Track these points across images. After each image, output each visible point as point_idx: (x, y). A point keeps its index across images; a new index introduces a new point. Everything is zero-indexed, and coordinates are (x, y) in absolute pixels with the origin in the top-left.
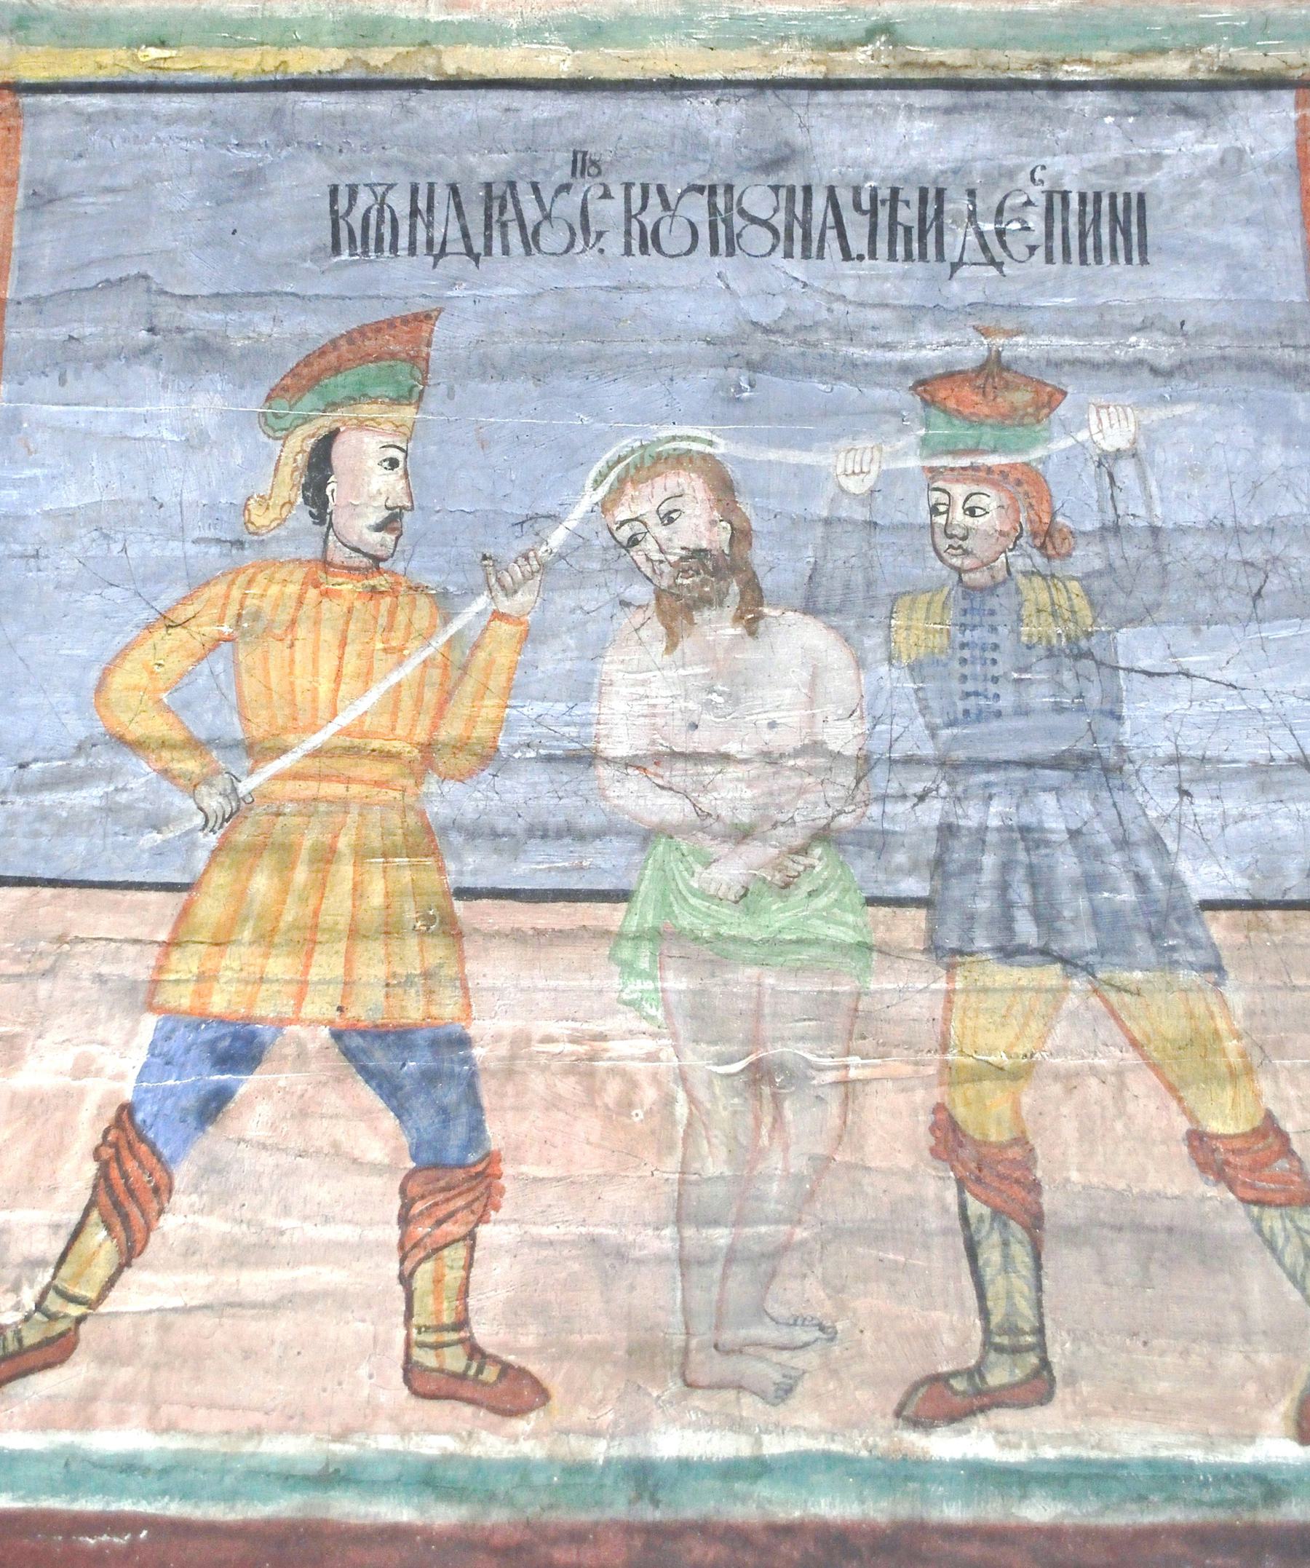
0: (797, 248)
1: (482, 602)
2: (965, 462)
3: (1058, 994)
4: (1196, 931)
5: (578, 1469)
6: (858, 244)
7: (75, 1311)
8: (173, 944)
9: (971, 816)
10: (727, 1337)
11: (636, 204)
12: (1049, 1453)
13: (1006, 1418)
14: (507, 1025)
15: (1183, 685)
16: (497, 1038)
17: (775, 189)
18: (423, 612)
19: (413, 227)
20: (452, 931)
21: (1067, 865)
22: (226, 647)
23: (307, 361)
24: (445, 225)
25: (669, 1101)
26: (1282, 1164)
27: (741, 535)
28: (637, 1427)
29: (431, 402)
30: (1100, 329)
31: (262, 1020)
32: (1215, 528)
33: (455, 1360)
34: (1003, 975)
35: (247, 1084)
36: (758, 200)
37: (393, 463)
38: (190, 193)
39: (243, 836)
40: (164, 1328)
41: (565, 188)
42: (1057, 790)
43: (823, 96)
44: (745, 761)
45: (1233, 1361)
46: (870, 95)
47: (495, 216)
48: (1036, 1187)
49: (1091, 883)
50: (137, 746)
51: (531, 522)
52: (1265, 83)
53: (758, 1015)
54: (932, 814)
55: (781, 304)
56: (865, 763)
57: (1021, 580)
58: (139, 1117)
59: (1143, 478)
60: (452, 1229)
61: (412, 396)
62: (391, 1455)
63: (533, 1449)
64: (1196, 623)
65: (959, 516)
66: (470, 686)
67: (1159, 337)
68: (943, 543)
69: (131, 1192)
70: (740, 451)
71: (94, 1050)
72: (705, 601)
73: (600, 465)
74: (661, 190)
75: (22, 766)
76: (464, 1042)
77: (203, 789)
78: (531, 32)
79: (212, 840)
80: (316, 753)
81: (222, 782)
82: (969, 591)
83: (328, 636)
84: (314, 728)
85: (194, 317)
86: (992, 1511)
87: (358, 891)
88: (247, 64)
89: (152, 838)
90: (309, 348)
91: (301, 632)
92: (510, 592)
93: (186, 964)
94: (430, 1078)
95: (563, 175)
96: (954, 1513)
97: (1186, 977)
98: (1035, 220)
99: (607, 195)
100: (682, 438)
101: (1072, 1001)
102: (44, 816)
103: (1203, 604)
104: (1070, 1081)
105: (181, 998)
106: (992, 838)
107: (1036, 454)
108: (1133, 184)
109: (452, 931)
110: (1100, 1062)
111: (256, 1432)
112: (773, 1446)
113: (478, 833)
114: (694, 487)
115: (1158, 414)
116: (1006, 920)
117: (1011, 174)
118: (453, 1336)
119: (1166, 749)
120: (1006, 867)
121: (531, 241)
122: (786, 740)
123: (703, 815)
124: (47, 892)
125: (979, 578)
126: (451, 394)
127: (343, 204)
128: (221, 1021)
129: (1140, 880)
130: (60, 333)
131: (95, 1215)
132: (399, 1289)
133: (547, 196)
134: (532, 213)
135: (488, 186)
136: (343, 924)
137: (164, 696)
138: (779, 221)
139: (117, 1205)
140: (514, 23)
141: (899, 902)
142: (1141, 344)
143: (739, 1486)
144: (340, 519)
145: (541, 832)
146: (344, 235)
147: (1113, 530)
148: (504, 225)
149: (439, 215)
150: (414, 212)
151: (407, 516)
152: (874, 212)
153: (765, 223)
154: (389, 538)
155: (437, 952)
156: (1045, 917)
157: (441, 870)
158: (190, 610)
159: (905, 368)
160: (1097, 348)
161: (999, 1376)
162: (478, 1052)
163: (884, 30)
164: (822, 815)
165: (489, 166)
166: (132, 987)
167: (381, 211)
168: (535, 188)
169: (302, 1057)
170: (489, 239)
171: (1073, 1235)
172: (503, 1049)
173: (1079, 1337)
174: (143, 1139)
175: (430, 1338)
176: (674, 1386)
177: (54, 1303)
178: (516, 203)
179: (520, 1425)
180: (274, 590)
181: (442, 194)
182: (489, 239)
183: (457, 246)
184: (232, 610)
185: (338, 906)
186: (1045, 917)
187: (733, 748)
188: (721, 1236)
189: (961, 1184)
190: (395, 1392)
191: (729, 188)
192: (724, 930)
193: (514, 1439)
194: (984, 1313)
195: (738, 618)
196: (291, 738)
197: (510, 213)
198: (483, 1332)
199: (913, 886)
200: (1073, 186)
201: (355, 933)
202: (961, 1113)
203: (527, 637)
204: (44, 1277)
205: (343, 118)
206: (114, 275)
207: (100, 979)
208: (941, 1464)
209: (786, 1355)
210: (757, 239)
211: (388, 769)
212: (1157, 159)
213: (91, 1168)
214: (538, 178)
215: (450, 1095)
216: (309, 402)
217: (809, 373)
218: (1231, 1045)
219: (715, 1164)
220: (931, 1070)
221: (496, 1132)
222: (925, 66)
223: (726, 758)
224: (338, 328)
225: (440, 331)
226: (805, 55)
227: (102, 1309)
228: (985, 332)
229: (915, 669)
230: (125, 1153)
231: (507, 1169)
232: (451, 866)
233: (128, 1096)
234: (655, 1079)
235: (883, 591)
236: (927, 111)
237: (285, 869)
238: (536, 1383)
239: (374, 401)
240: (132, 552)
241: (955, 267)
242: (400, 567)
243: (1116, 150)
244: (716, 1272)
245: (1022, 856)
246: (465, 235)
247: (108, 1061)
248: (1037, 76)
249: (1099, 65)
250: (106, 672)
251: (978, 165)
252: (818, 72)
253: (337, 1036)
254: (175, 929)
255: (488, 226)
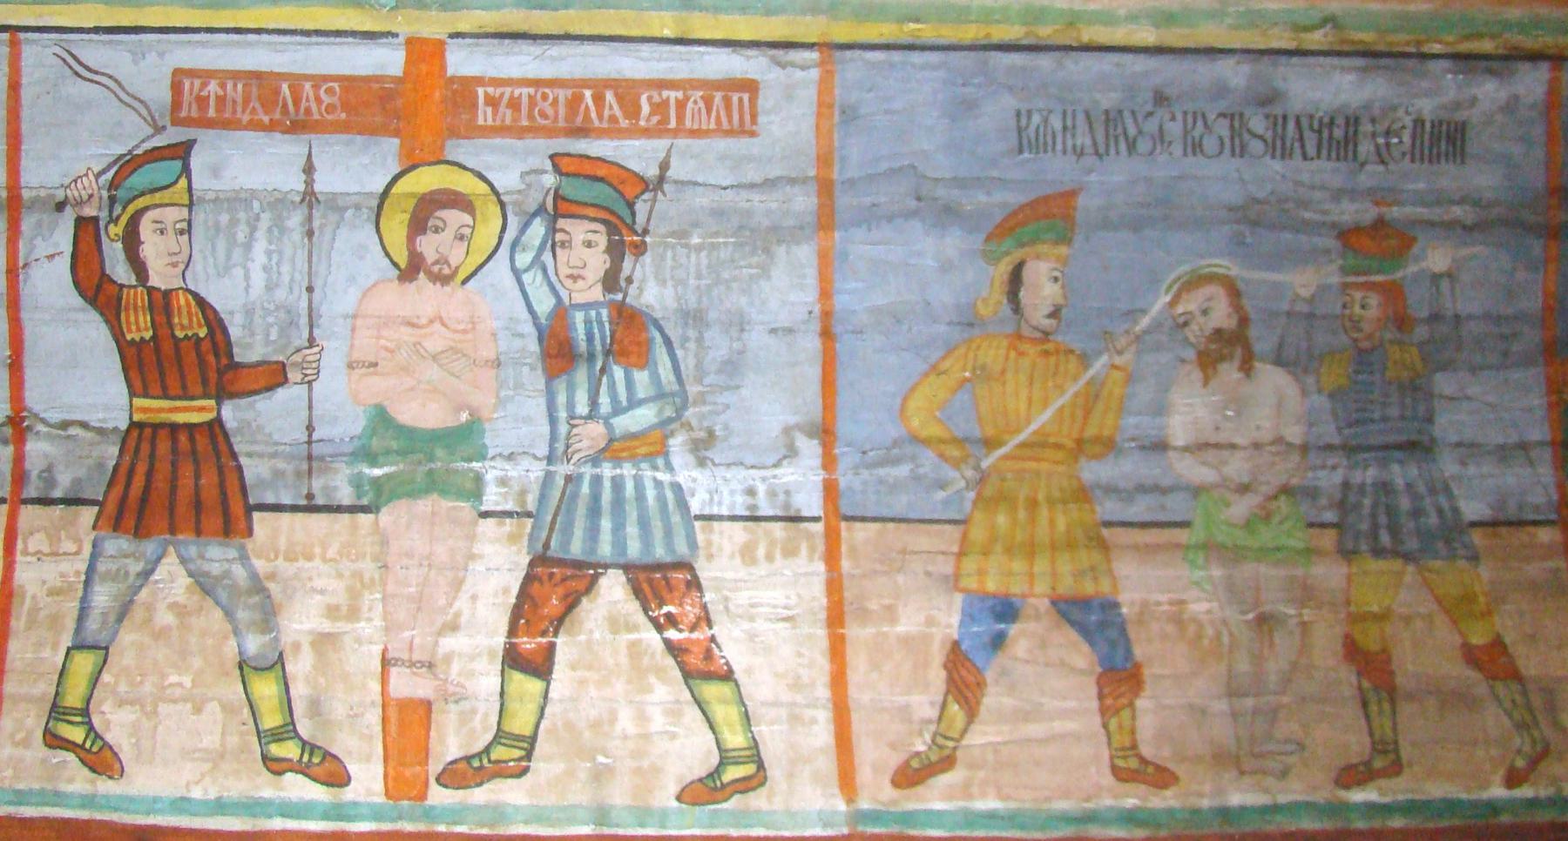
0: (1278, 152)
1: (1104, 359)
2: (1361, 279)
3: (1400, 574)
4: (1466, 539)
5: (1196, 811)
6: (1311, 150)
7: (951, 744)
8: (961, 554)
9: (1357, 477)
10: (1257, 750)
11: (1190, 126)
12: (1401, 797)
13: (1383, 782)
14: (1137, 596)
15: (1465, 404)
16: (1132, 603)
17: (1267, 117)
18: (1073, 364)
19: (1064, 137)
20: (1104, 546)
21: (1405, 504)
22: (968, 385)
23: (1005, 220)
24: (1083, 139)
25: (1218, 636)
26: (1503, 659)
27: (1244, 321)
28: (1220, 791)
29: (1076, 245)
30: (1438, 203)
31: (1015, 595)
32: (1487, 317)
33: (1133, 763)
34: (1374, 565)
35: (1014, 630)
36: (1258, 124)
37: (1056, 279)
38: (935, 114)
39: (989, 491)
40: (996, 751)
41: (1150, 114)
42: (1400, 462)
43: (1295, 60)
44: (1245, 448)
45: (1480, 753)
46: (1321, 59)
47: (1111, 131)
48: (1392, 673)
49: (1417, 513)
50: (926, 442)
51: (1132, 314)
52: (1534, 57)
53: (1258, 589)
54: (1338, 477)
55: (1269, 187)
56: (1304, 449)
57: (1387, 346)
58: (963, 647)
59: (1452, 289)
60: (1124, 701)
61: (1065, 239)
62: (1111, 808)
63: (1173, 803)
64: (1474, 370)
65: (1357, 310)
66: (1100, 406)
67: (1467, 208)
68: (1348, 324)
69: (967, 686)
70: (1246, 274)
71: (935, 612)
72: (1222, 358)
73: (1168, 281)
74: (1204, 116)
75: (864, 453)
76: (1116, 605)
77: (963, 466)
78: (1132, 18)
79: (971, 495)
80: (1023, 445)
81: (972, 461)
82: (1361, 351)
83: (1023, 378)
84: (1018, 431)
85: (941, 192)
86: (1377, 824)
87: (1052, 522)
88: (969, 34)
89: (940, 495)
90: (1008, 211)
91: (1009, 376)
92: (1120, 353)
93: (970, 564)
94: (1103, 625)
95: (1149, 107)
96: (1360, 824)
97: (1462, 563)
98: (1406, 138)
99: (1173, 119)
100: (1216, 266)
101: (1408, 578)
102: (881, 481)
103: (1478, 358)
104: (1407, 620)
105: (971, 583)
106: (1369, 489)
107: (1399, 275)
108: (1461, 116)
109: (1104, 546)
110: (1421, 610)
111: (1048, 799)
112: (1282, 799)
113: (1111, 490)
114: (1216, 290)
115: (1464, 252)
116: (1374, 532)
117: (1394, 108)
118: (1130, 753)
119: (1454, 438)
120: (1375, 505)
121: (1132, 146)
122: (1266, 436)
123: (1224, 479)
124: (891, 525)
125: (1365, 344)
126: (1087, 239)
127: (1024, 122)
128: (995, 596)
129: (1440, 512)
130: (868, 200)
131: (950, 698)
132: (1102, 730)
133: (1140, 119)
134: (1132, 131)
135: (1107, 112)
136: (1047, 540)
137: (937, 414)
138: (1269, 135)
139: (960, 692)
140: (1122, 12)
141: (1323, 525)
142: (1457, 211)
143: (1268, 817)
144: (1028, 311)
145: (1142, 489)
146: (1025, 142)
147: (1435, 318)
148: (1116, 137)
149: (1079, 131)
150: (1065, 128)
151: (1064, 311)
152: (1320, 132)
153: (1261, 137)
154: (1053, 322)
155: (1097, 557)
156: (1394, 531)
157: (1093, 511)
158: (946, 364)
159: (1334, 225)
160: (1435, 214)
161: (732, 773)
162: (1124, 610)
163: (1330, 20)
164: (1283, 479)
165: (1108, 100)
166: (946, 578)
167: (1045, 127)
168: (1133, 113)
169: (1037, 617)
170: (1107, 146)
171: (1411, 697)
172: (1136, 609)
173: (1413, 744)
174: (969, 660)
175: (1120, 754)
176: (1235, 773)
177: (940, 740)
178: (1123, 123)
179: (1168, 793)
180: (992, 352)
181: (1081, 117)
182: (1107, 146)
183: (1089, 150)
184: (969, 366)
185: (1042, 532)
186: (1394, 531)
187: (1238, 440)
188: (1249, 702)
189: (1359, 673)
190: (1108, 780)
191: (1241, 115)
192: (1238, 543)
193: (1165, 799)
194: (1371, 734)
195: (1241, 369)
196: (1006, 437)
197: (1120, 130)
198: (1146, 750)
199: (1330, 516)
200: (1428, 116)
201: (1053, 547)
202: (1358, 637)
203: (1130, 379)
204: (933, 728)
205: (1023, 69)
206: (896, 165)
207: (928, 574)
208: (1356, 804)
209: (1284, 757)
210: (1256, 146)
211: (1060, 455)
212: (1473, 101)
213: (943, 674)
214: (1136, 108)
215: (1113, 633)
216: (1008, 243)
217: (1284, 228)
218: (1482, 599)
219: (1243, 666)
220: (1343, 616)
221: (1138, 652)
222: (1353, 42)
223: (1233, 446)
224: (1022, 199)
225: (1081, 201)
226: (1286, 35)
227: (964, 742)
228: (1377, 204)
229: (1331, 396)
230: (959, 665)
231: (1146, 672)
232: (1098, 509)
233: (956, 637)
234: (1212, 622)
235: (1317, 352)
236: (1349, 70)
237: (1013, 509)
238: (1173, 774)
239: (1044, 242)
240: (915, 328)
241: (1363, 165)
242: (1060, 338)
243: (1452, 94)
244: (1249, 719)
245: (1383, 499)
246: (1095, 144)
247: (941, 617)
248: (1413, 50)
249: (1447, 44)
250: (905, 400)
251: (1377, 104)
252: (1292, 45)
253: (1054, 603)
254: (962, 546)
255: (1107, 137)
